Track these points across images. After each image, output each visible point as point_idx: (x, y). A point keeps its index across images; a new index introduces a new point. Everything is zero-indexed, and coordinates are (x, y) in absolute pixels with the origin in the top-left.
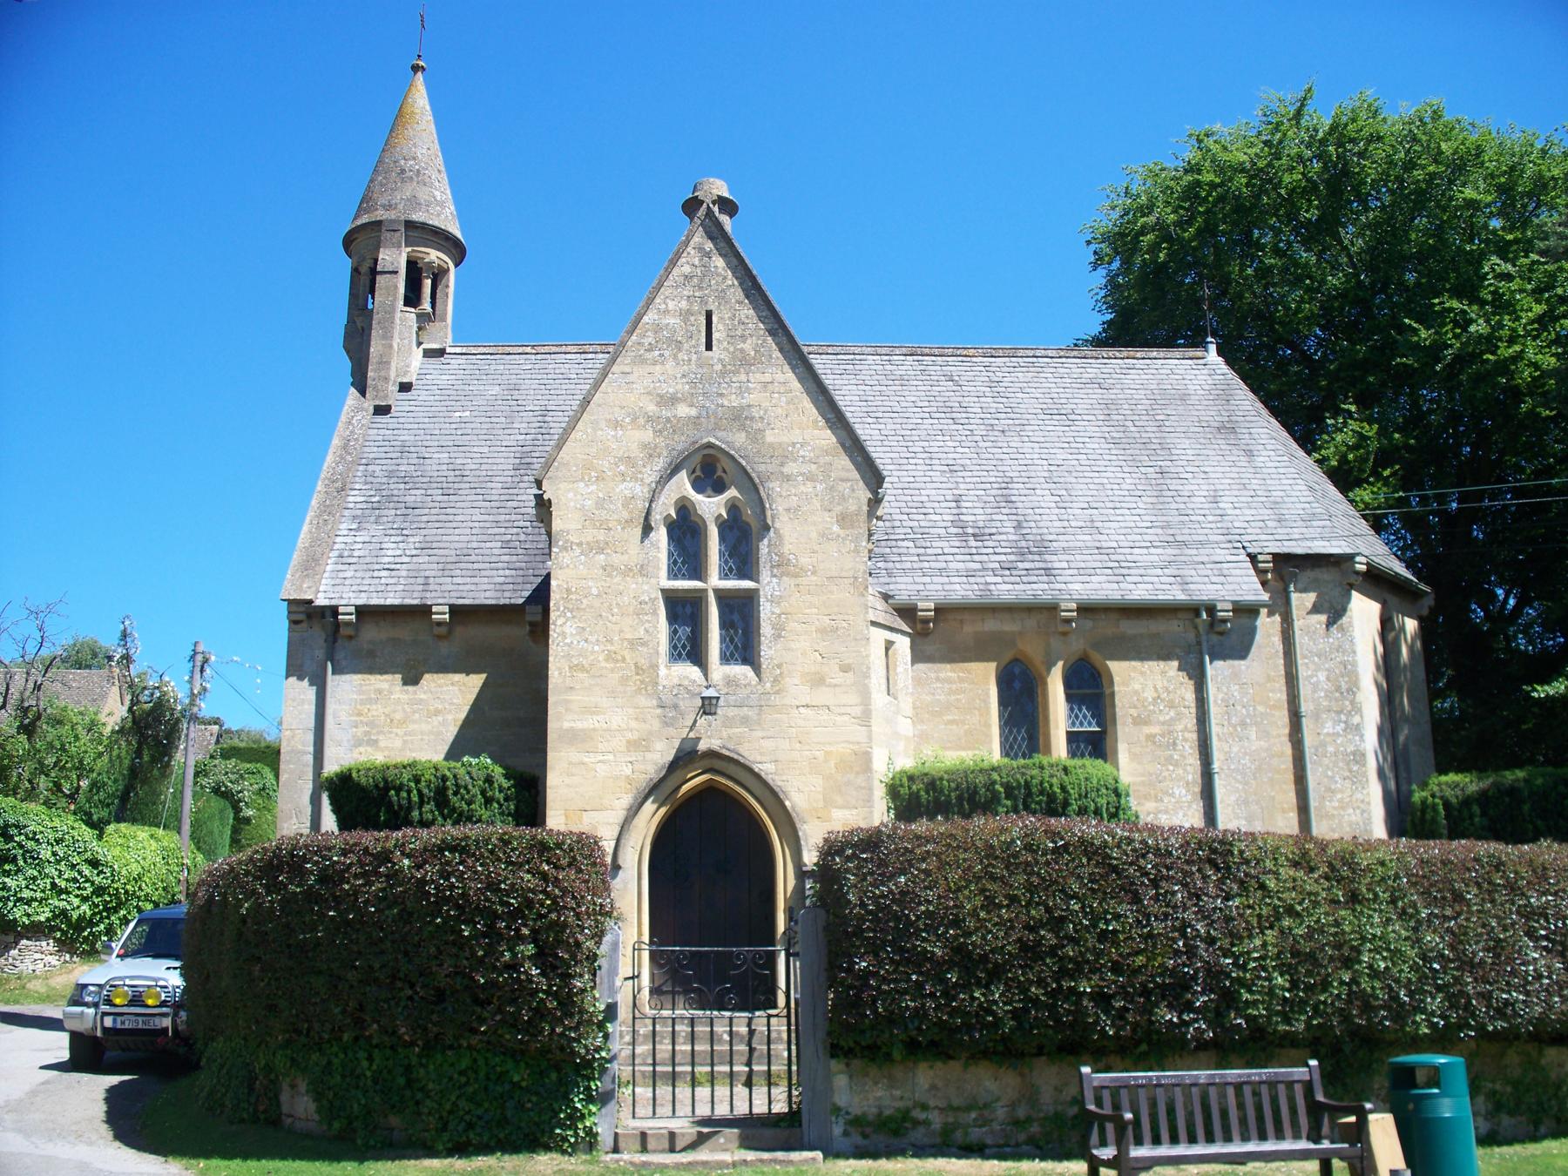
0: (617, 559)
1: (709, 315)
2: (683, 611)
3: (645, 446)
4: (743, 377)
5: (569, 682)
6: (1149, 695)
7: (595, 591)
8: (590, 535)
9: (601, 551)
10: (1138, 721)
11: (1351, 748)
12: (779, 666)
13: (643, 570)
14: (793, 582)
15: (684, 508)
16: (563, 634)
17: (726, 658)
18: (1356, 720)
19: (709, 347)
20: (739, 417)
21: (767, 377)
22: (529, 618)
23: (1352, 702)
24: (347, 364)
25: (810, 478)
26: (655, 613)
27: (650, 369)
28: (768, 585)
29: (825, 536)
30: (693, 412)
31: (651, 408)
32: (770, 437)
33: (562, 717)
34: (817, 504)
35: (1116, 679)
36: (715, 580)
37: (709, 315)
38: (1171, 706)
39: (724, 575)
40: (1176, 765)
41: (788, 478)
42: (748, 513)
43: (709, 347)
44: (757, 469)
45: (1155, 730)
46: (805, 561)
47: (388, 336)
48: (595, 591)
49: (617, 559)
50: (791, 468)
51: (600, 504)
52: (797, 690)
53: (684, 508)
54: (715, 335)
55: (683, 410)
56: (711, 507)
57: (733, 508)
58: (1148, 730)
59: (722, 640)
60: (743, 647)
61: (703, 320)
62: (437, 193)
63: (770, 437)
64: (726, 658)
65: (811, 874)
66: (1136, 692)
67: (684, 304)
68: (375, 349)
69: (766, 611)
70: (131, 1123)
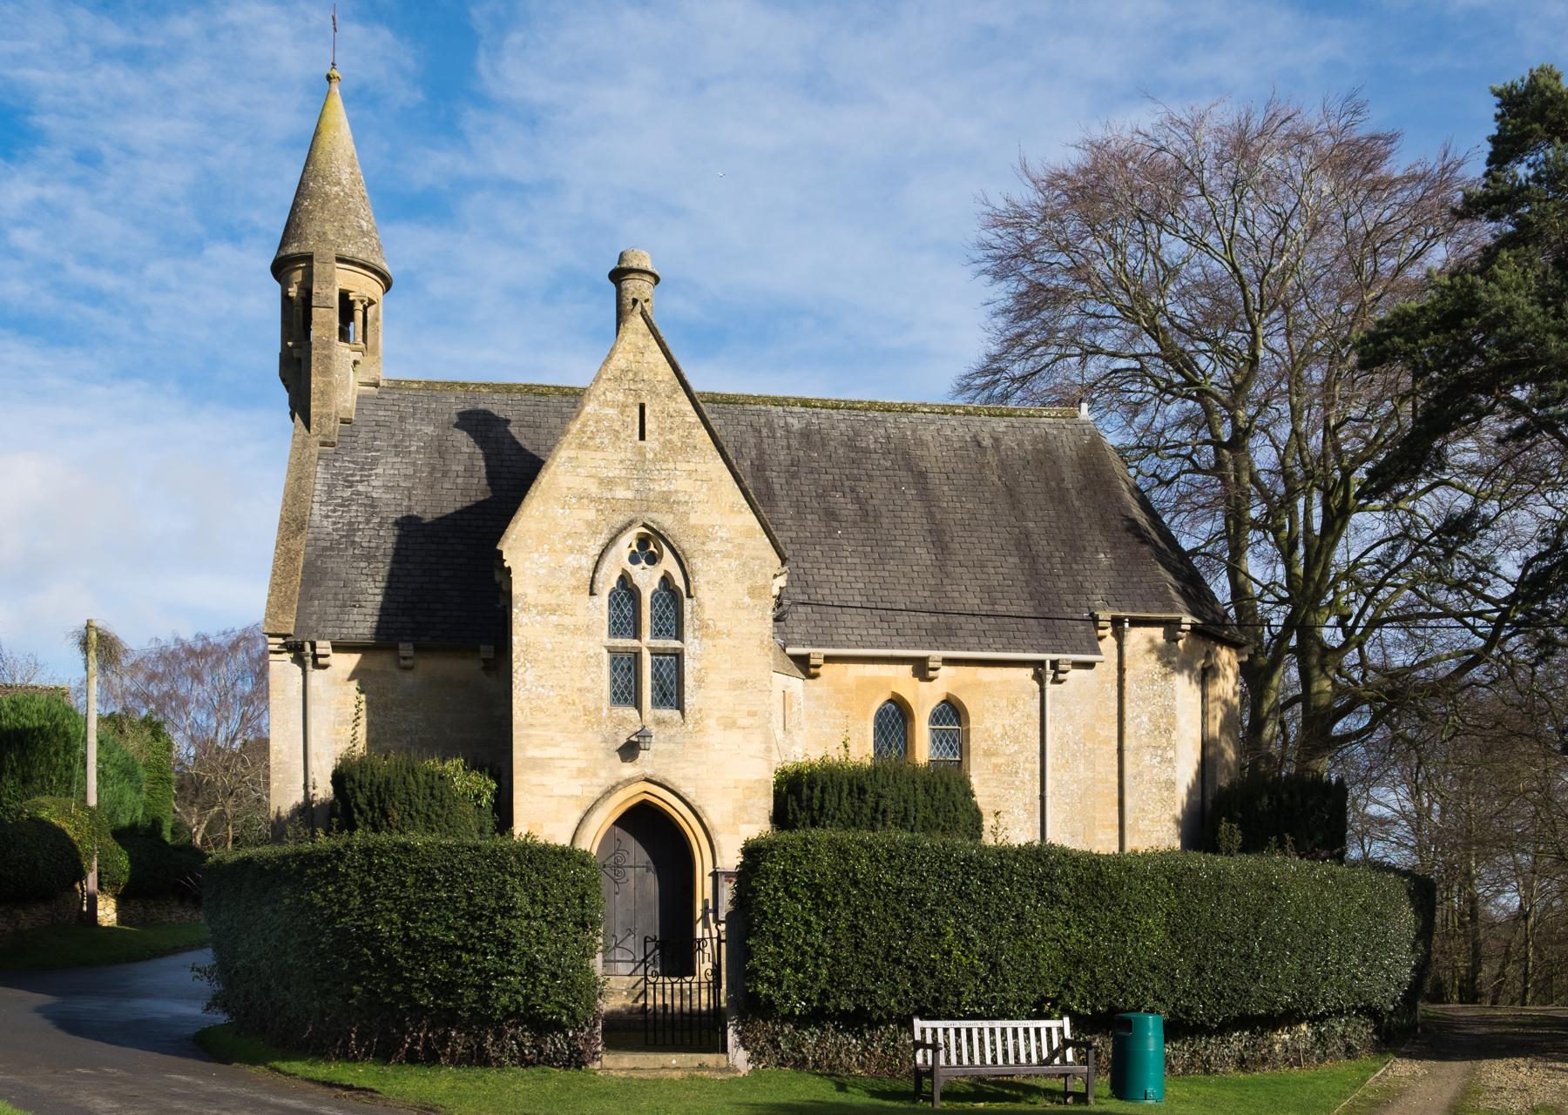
0: (567, 621)
1: (642, 408)
2: (625, 670)
3: (589, 524)
4: (671, 466)
5: (529, 720)
6: (998, 731)
7: (549, 646)
8: (545, 598)
9: (553, 612)
10: (988, 754)
11: (1163, 777)
12: (700, 710)
13: (588, 630)
14: (710, 643)
15: (625, 579)
16: (523, 680)
17: (656, 703)
18: (1170, 754)
19: (642, 437)
20: (666, 499)
21: (691, 466)
22: (483, 656)
23: (1169, 740)
24: (284, 396)
25: (727, 555)
26: (599, 666)
27: (593, 454)
28: (691, 645)
29: (738, 606)
30: (629, 495)
31: (594, 490)
32: (694, 519)
33: (525, 748)
34: (731, 576)
35: (972, 719)
36: (647, 641)
37: (642, 408)
38: (1016, 740)
39: (657, 634)
40: (1017, 788)
41: (708, 554)
42: (679, 582)
43: (642, 437)
44: (686, 545)
45: (1001, 760)
46: (721, 625)
47: (327, 371)
48: (549, 646)
49: (567, 621)
50: (711, 546)
51: (553, 572)
52: (715, 735)
53: (625, 579)
54: (648, 426)
55: (622, 493)
56: (647, 579)
57: (666, 580)
58: (994, 760)
59: (653, 690)
60: (671, 693)
61: (637, 410)
62: (364, 223)
63: (694, 519)
64: (656, 703)
65: (728, 875)
66: (987, 729)
67: (621, 397)
68: (316, 382)
69: (689, 665)
70: (881, 715)
